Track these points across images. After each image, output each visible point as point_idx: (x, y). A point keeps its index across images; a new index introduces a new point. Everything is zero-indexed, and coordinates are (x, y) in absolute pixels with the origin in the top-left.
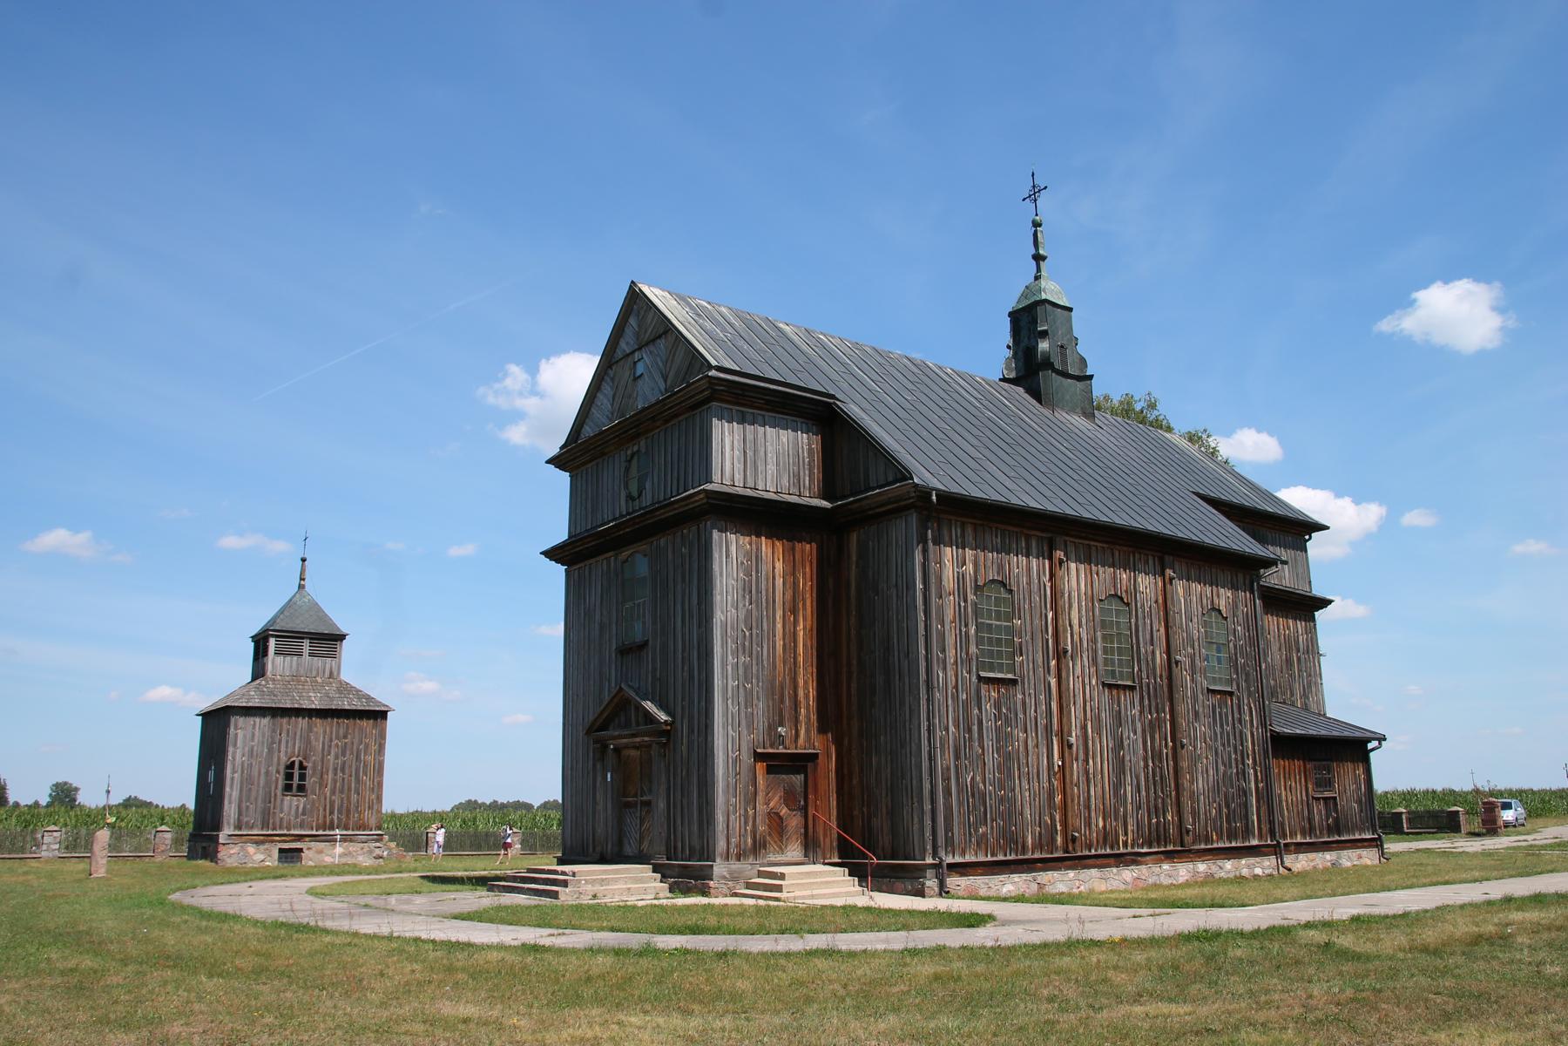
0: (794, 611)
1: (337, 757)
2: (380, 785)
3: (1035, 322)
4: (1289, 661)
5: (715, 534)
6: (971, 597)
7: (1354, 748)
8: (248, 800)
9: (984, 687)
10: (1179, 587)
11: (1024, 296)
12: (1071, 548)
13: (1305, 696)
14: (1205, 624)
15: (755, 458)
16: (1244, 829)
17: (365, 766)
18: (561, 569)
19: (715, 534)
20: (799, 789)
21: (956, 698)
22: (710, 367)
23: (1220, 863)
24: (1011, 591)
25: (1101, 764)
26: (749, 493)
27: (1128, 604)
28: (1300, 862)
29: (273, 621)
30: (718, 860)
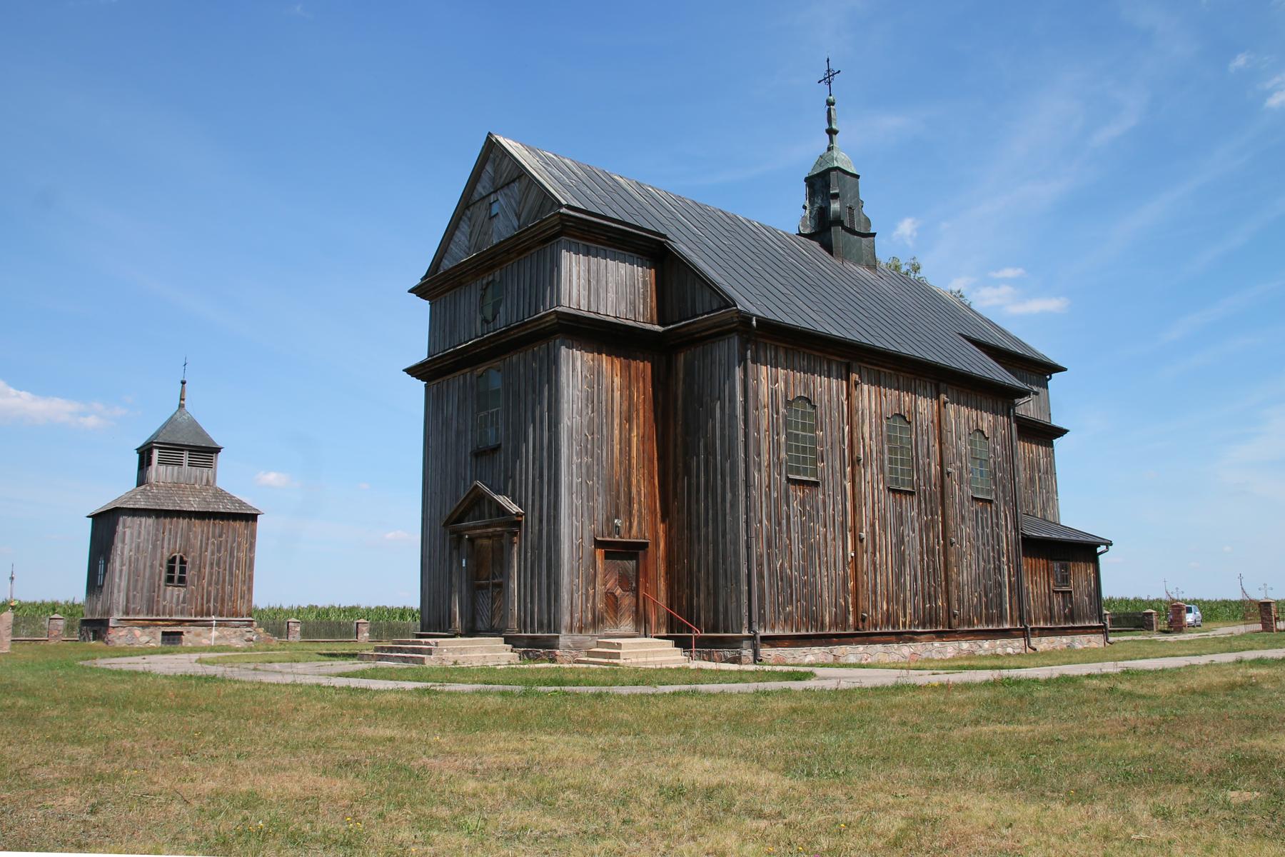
0: (629, 420)
1: (213, 554)
2: (251, 578)
3: (828, 186)
4: (1032, 480)
5: (564, 350)
6: (782, 410)
7: (1085, 551)
8: (135, 589)
9: (791, 487)
10: (951, 409)
11: (818, 163)
12: (864, 373)
13: (1044, 509)
14: (971, 443)
15: (597, 285)
16: (997, 618)
17: (238, 561)
18: (421, 385)
19: (564, 350)
20: (632, 573)
21: (769, 496)
22: (561, 205)
23: (979, 642)
24: (815, 407)
25: (885, 557)
26: (592, 315)
27: (909, 423)
28: (1043, 644)
29: (157, 434)
30: (563, 632)
